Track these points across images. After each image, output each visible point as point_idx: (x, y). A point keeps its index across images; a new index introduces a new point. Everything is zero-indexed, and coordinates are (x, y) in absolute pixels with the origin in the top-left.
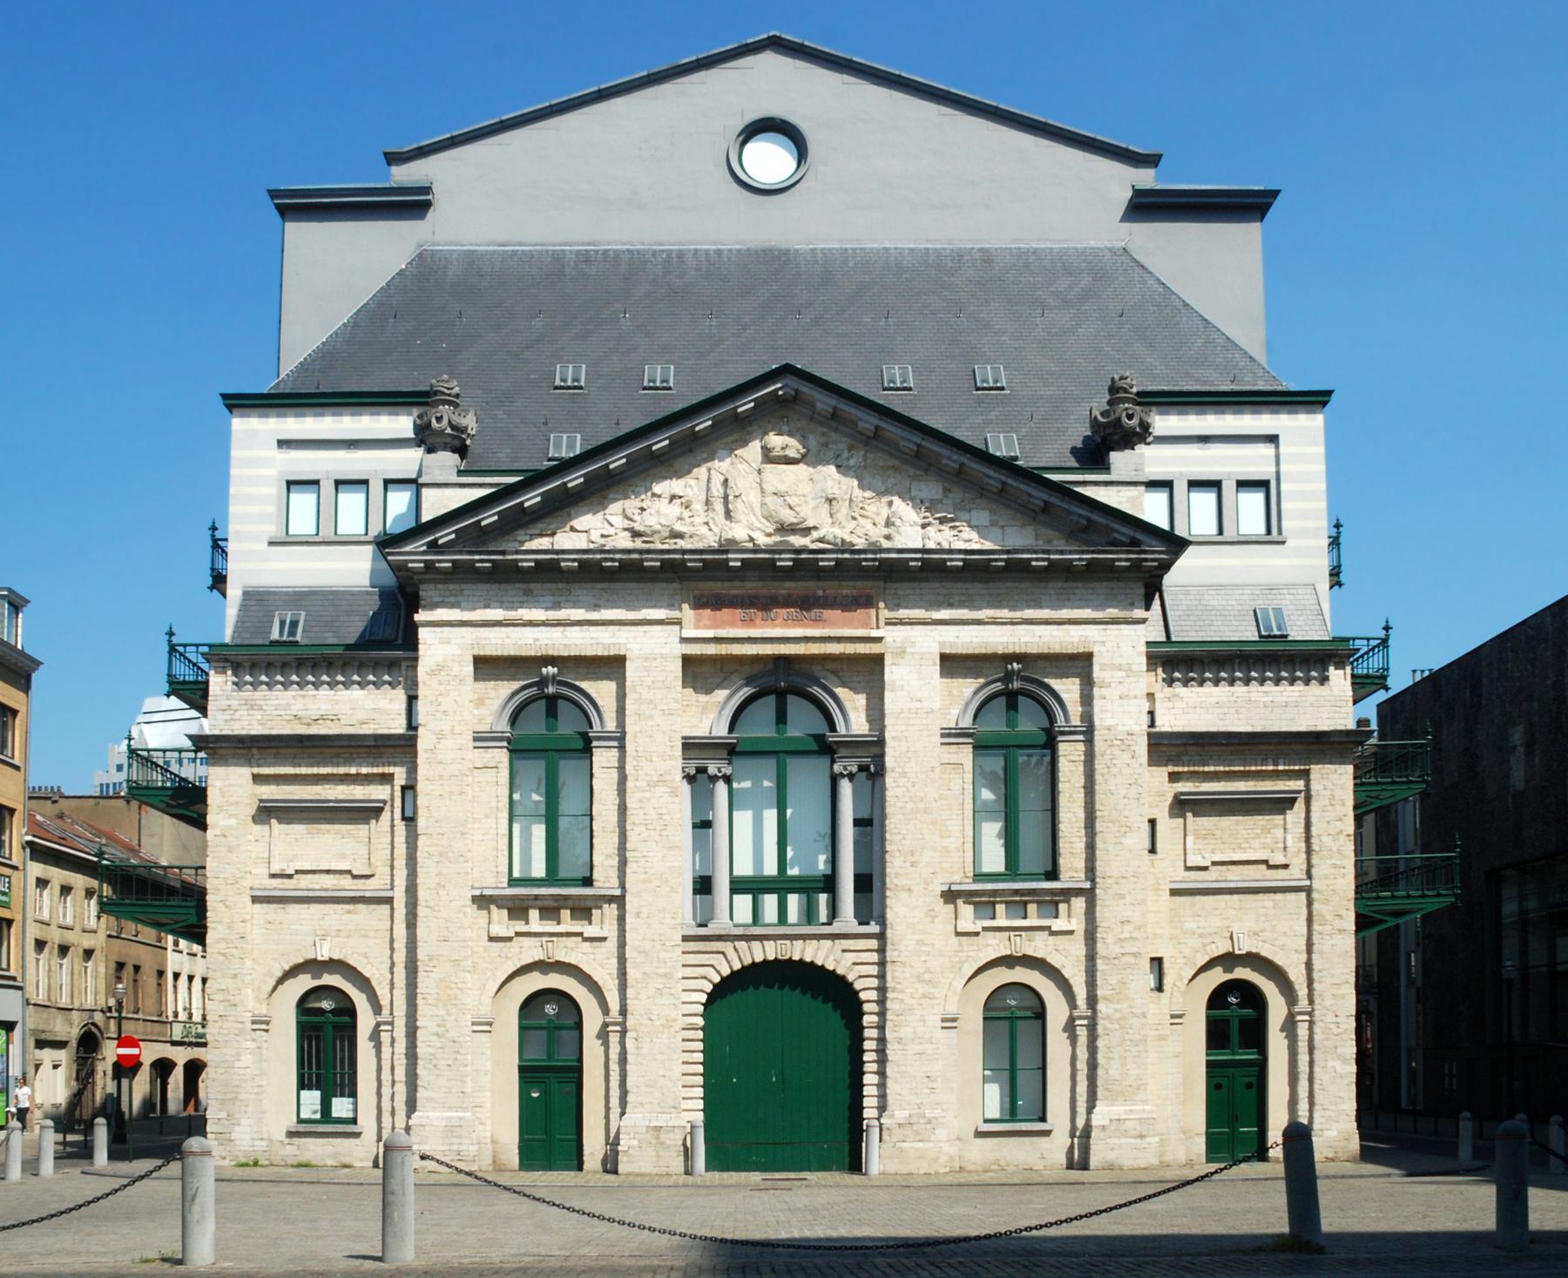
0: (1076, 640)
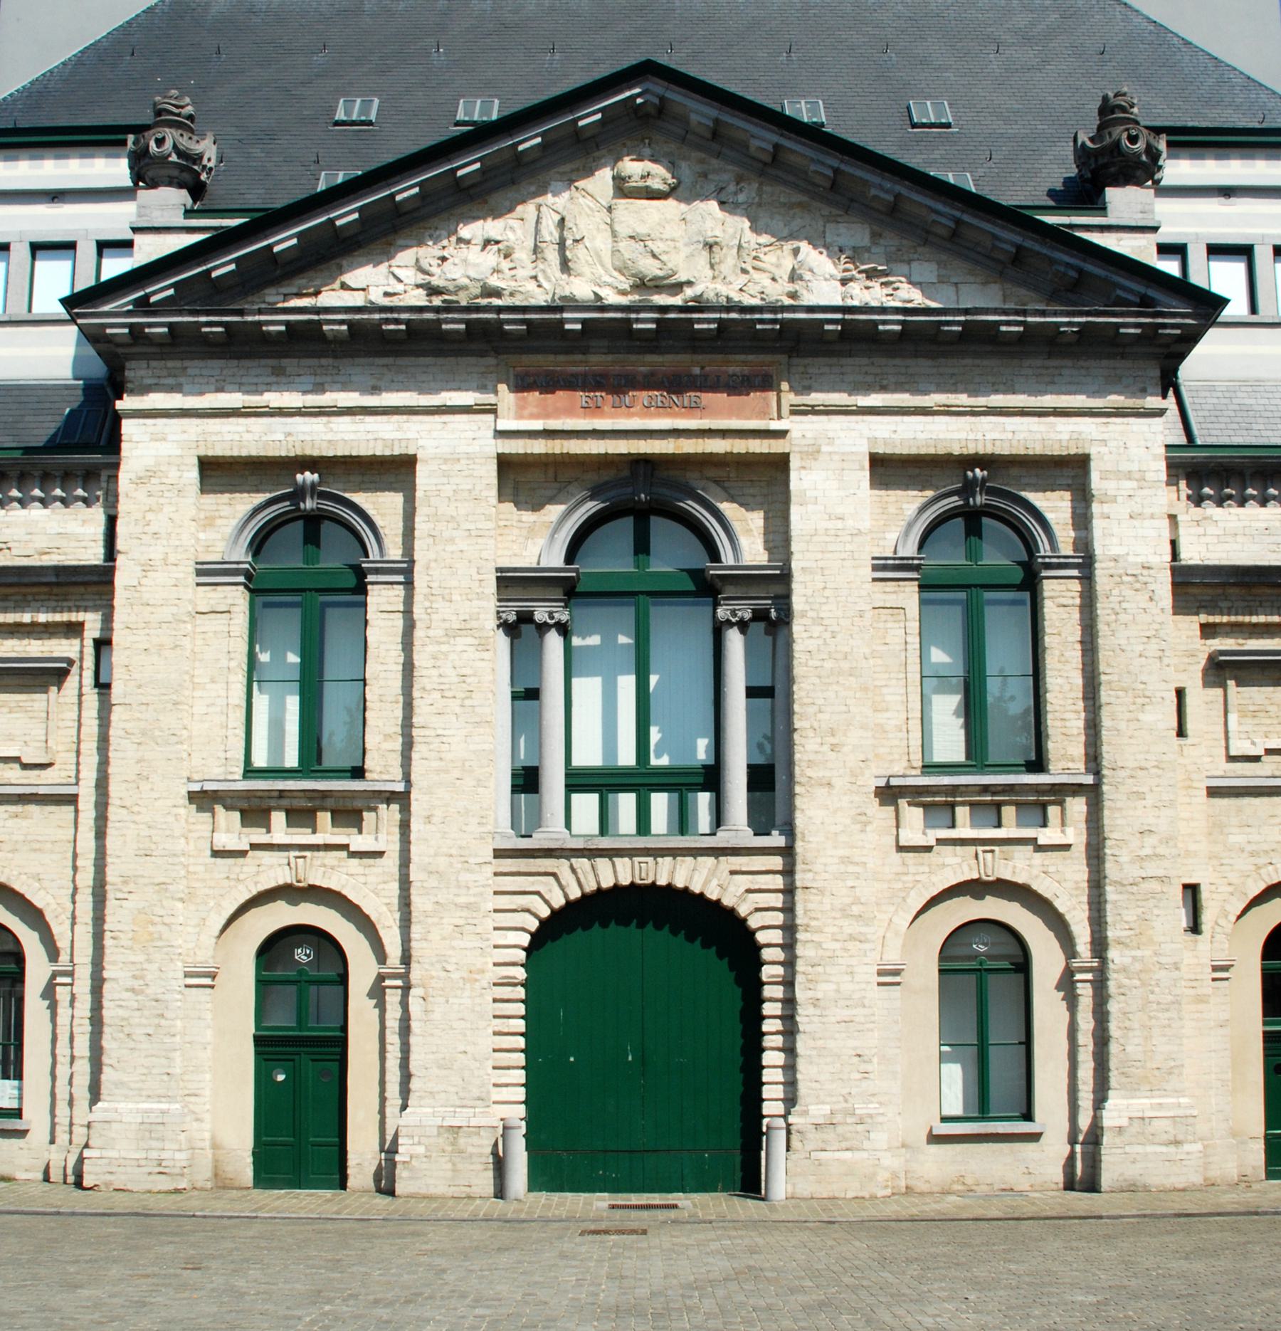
0: (1065, 437)
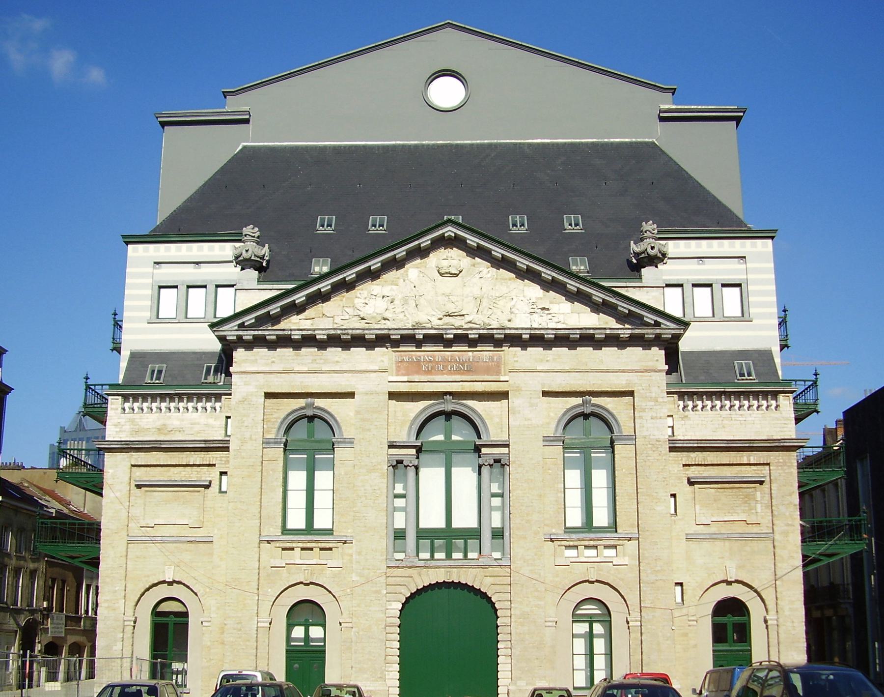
0: (624, 382)
